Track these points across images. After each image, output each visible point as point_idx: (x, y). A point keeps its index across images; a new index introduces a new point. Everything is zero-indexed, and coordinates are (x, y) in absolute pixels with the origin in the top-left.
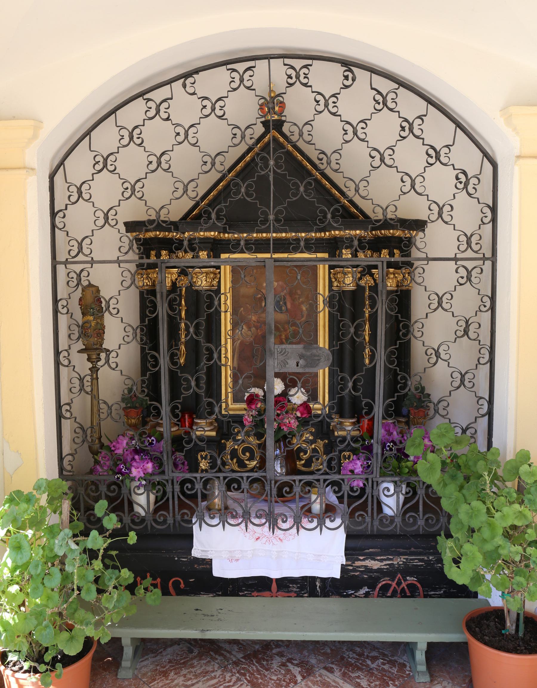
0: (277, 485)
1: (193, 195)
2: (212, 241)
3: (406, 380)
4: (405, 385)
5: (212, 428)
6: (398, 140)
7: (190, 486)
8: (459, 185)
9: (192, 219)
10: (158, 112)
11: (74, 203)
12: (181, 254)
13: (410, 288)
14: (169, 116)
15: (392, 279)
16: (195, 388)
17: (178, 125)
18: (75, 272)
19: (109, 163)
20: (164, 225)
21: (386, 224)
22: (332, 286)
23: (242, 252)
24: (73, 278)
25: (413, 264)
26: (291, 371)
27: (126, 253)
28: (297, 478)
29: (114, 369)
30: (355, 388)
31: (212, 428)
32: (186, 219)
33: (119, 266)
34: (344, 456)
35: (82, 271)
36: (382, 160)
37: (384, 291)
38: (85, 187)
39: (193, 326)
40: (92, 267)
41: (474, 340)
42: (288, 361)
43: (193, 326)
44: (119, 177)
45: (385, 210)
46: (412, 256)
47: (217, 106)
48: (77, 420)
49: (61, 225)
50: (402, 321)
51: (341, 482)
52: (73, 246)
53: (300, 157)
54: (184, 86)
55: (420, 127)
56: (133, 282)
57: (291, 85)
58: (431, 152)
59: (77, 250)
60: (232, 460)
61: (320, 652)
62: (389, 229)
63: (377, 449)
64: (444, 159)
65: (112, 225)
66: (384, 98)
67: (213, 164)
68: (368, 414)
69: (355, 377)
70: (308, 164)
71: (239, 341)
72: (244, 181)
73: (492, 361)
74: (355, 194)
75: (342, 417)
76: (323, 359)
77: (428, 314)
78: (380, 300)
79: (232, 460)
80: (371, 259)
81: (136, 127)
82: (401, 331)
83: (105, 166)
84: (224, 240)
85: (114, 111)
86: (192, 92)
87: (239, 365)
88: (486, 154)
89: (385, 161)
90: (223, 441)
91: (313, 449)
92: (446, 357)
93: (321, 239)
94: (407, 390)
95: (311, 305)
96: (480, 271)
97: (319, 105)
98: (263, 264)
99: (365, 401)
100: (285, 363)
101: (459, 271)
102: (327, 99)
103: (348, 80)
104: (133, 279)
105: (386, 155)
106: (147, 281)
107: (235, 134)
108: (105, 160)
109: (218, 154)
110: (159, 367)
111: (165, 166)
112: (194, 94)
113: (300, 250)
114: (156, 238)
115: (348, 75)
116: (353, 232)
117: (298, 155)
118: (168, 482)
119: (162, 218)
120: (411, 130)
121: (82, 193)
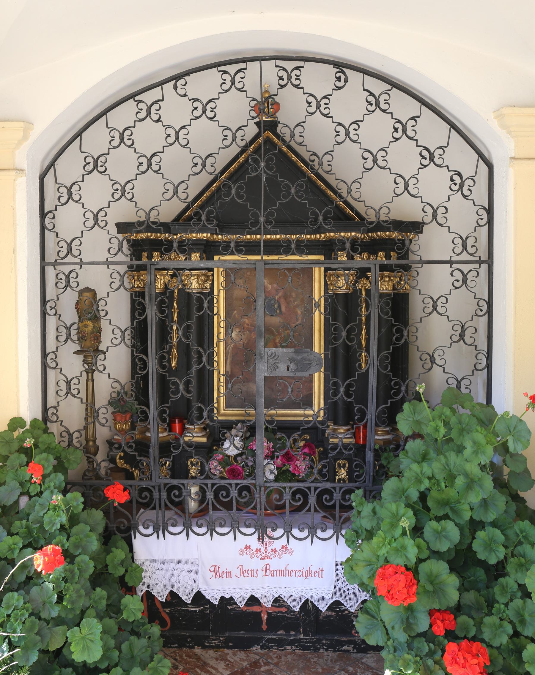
1: (184, 196)
2: (205, 242)
5: (204, 434)
6: (391, 142)
7: (177, 492)
8: (453, 187)
9: (184, 220)
10: (149, 113)
11: (63, 204)
12: (173, 255)
14: (160, 118)
16: (184, 393)
17: (168, 126)
18: (64, 273)
19: (99, 164)
20: (154, 226)
21: (379, 226)
22: (328, 289)
23: (232, 254)
24: (61, 279)
25: (411, 266)
26: (281, 375)
27: (115, 255)
28: (287, 485)
29: (101, 372)
30: (347, 393)
31: (204, 434)
32: (178, 221)
33: (108, 268)
34: (339, 464)
35: (71, 272)
36: (375, 161)
38: (75, 188)
40: (81, 268)
41: (471, 345)
42: (278, 365)
44: (110, 178)
45: (378, 212)
46: (409, 259)
47: (208, 107)
48: (63, 424)
49: (50, 226)
50: (396, 325)
51: (333, 490)
52: (62, 247)
53: (294, 158)
54: (175, 87)
55: (413, 128)
56: (122, 284)
57: (283, 86)
59: (66, 251)
61: (311, 671)
62: (385, 232)
64: (438, 161)
65: (102, 226)
67: (204, 166)
68: (361, 420)
69: (347, 382)
70: (303, 165)
71: (233, 345)
72: (235, 183)
73: (489, 367)
75: (335, 424)
76: (314, 364)
77: (423, 319)
78: (373, 304)
80: (368, 262)
81: (127, 129)
82: (394, 335)
83: (96, 167)
84: (218, 242)
85: (105, 113)
86: (183, 93)
87: (231, 369)
88: (481, 155)
90: (214, 448)
92: (441, 363)
93: (316, 241)
96: (476, 274)
97: (311, 106)
98: (253, 266)
99: (357, 407)
102: (319, 100)
103: (340, 81)
104: (122, 281)
105: (379, 157)
106: (138, 283)
107: (226, 136)
108: (96, 161)
109: (209, 156)
111: (155, 167)
112: (185, 95)
113: (291, 253)
115: (340, 77)
116: (348, 234)
117: (293, 156)
118: (155, 488)
119: (152, 219)
120: (404, 131)
121: (72, 194)
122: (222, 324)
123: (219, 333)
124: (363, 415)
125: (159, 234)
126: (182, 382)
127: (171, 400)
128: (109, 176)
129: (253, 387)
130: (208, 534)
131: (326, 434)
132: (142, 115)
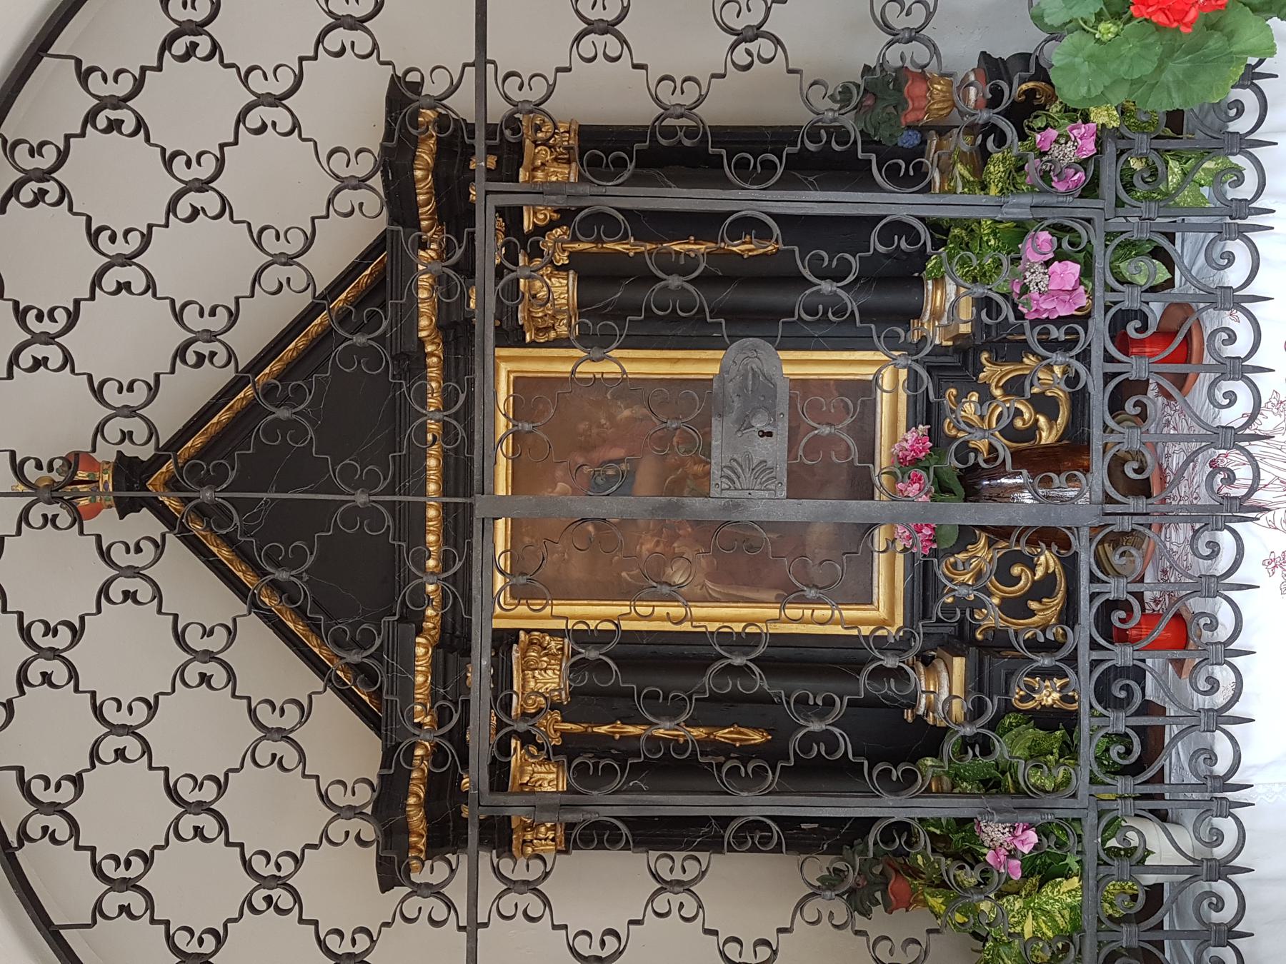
0: (1119, 497)
5: (941, 666)
14: (68, 778)
15: (547, 175)
17: (94, 756)
27: (450, 905)
29: (775, 952)
31: (941, 666)
33: (485, 925)
36: (203, 186)
37: (587, 189)
42: (755, 462)
47: (45, 642)
53: (223, 416)
58: (180, 47)
60: (1032, 613)
62: (413, 181)
63: (1018, 206)
66: (28, 177)
69: (806, 273)
71: (709, 584)
74: (299, 265)
75: (918, 314)
79: (1032, 613)
90: (979, 637)
91: (1006, 393)
93: (445, 365)
95: (616, 397)
100: (764, 468)
102: (29, 337)
104: (523, 888)
106: (543, 829)
110: (769, 822)
111: (210, 791)
114: (428, 805)
117: (215, 420)
122: (646, 611)
123: (668, 618)
124: (899, 227)
125: (414, 775)
127: (850, 756)
129: (818, 535)
130: (1238, 661)
131: (944, 343)
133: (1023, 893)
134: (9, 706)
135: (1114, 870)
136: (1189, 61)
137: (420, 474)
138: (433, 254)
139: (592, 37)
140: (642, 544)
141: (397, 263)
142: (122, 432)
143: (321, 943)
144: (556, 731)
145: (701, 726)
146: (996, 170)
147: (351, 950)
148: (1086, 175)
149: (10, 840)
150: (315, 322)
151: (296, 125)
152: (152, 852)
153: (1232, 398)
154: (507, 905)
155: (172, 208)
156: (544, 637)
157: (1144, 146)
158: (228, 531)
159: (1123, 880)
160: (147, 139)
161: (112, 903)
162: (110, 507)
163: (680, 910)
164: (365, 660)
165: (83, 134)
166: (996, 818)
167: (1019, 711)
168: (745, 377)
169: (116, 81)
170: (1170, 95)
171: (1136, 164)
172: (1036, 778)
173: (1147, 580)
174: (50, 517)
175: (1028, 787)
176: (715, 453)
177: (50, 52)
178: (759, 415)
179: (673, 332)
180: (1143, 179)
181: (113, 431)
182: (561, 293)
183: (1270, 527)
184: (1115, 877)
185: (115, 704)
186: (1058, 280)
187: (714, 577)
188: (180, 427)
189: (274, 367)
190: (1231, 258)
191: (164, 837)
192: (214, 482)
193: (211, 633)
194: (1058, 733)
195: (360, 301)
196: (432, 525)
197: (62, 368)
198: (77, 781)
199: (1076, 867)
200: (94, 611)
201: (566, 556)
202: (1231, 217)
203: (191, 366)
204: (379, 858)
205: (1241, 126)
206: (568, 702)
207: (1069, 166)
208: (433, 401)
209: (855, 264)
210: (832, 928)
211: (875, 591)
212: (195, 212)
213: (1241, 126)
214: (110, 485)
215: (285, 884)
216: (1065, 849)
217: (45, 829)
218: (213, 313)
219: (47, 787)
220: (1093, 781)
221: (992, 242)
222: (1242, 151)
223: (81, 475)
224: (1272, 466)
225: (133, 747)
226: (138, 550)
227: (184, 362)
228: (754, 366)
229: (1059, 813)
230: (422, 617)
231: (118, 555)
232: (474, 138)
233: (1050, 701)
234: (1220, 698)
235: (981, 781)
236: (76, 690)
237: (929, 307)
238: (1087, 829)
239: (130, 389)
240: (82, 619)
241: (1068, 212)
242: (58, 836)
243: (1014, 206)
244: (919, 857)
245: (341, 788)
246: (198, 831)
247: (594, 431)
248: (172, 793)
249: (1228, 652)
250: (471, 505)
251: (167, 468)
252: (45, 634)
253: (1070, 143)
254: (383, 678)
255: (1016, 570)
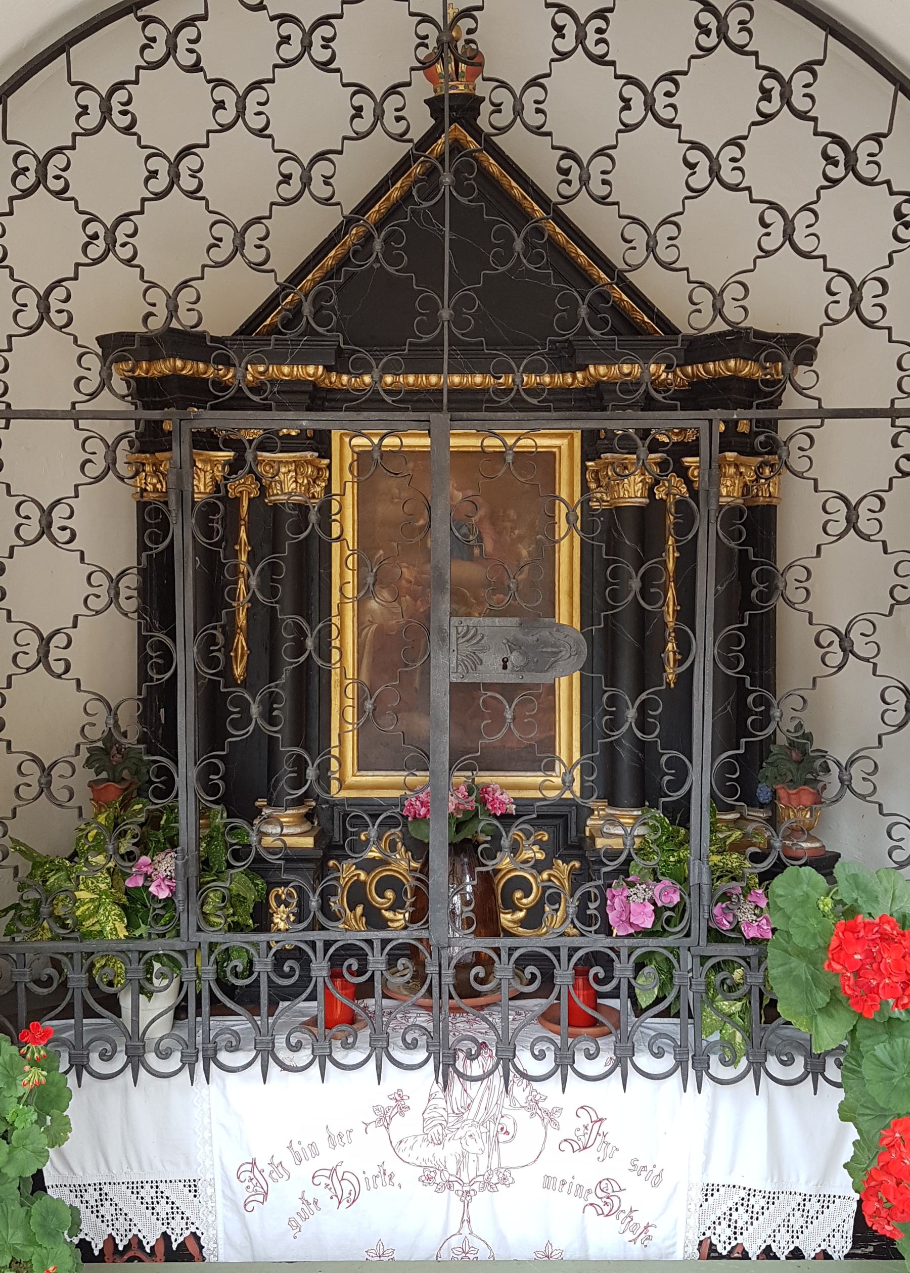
3: (769, 705)
4: (765, 720)
10: (172, 50)
13: (775, 501)
17: (220, 82)
19: (52, 171)
27: (93, 395)
29: (59, 676)
30: (643, 724)
31: (306, 827)
33: (77, 426)
36: (715, 172)
37: (713, 507)
39: (257, 572)
42: (481, 655)
43: (257, 572)
47: (317, 38)
53: (517, 191)
55: (807, 90)
60: (352, 909)
62: (725, 359)
63: (700, 873)
66: (722, 21)
69: (643, 696)
71: (374, 627)
74: (647, 257)
75: (612, 804)
76: (565, 654)
79: (352, 909)
83: (41, 179)
85: (62, 47)
89: (722, 173)
90: (331, 863)
93: (566, 390)
94: (769, 731)
95: (539, 543)
101: (900, 442)
102: (582, 22)
105: (724, 160)
106: (155, 481)
108: (43, 164)
110: (172, 670)
114: (175, 377)
117: (514, 184)
120: (786, 99)
126: (258, 698)
128: (76, 203)
129: (419, 723)
130: (315, 1069)
131: (587, 829)
132: (156, 52)
133: (113, 890)
134: (260, 7)
135: (135, 965)
136: (807, 978)
137: (468, 368)
138: (664, 376)
139: (844, 510)
140: (408, 568)
141: (653, 345)
142: (501, 104)
143: (58, 283)
144: (241, 492)
145: (247, 621)
146: (733, 860)
147: (53, 310)
148: (727, 930)
149: (143, 9)
150: (601, 273)
151: (768, 254)
152: (135, 134)
153: (540, 1057)
154: (94, 445)
155: (695, 146)
156: (324, 481)
157: (753, 980)
158: (416, 197)
159: (126, 972)
160: (754, 124)
161: (90, 99)
162: (435, 91)
163: (94, 595)
164: (305, 319)
165: (758, 67)
166: (180, 862)
167: (268, 894)
168: (554, 645)
169: (804, 96)
170: (781, 965)
171: (738, 974)
172: (214, 898)
173: (386, 1002)
174: (426, 41)
175: (205, 891)
176: (488, 621)
177: (829, 36)
178: (521, 658)
179: (595, 592)
180: (724, 979)
181: (502, 95)
182: (628, 492)
183: (430, 1095)
184: (128, 967)
185: (263, 100)
186: (639, 910)
187: (380, 632)
188: (507, 153)
189: (561, 236)
190: (659, 1055)
191: (148, 144)
192: (458, 185)
193: (327, 183)
194: (251, 922)
195: (617, 310)
196: (423, 379)
197: (556, 51)
198: (196, 68)
199: (137, 933)
200: (344, 81)
201: (396, 500)
202: (694, 1055)
203: (558, 164)
204: (132, 335)
205: (773, 1064)
206: (266, 504)
207: (735, 916)
208: (531, 380)
209: (649, 738)
210: (81, 725)
211: (370, 773)
212: (692, 166)
213: (773, 1064)
214: (455, 91)
215: (109, 250)
216: (153, 924)
217: (154, 40)
218: (605, 182)
219: (191, 41)
220: (212, 946)
221: (672, 859)
222: (751, 1064)
223: (463, 67)
224: (483, 1096)
225: (225, 116)
226: (398, 119)
227: (562, 157)
228: (563, 653)
229: (184, 917)
230: (340, 373)
231: (394, 101)
232: (757, 408)
233: (276, 920)
234: (284, 1054)
235: (207, 859)
236: (276, 66)
237: (618, 812)
238: (171, 941)
239: (538, 111)
240: (338, 70)
241: (695, 915)
242: (147, 51)
243: (700, 869)
244: (141, 806)
245: (194, 299)
246: (153, 174)
247: (508, 524)
248: (187, 151)
249: (323, 1059)
250: (439, 410)
251: (471, 142)
252: (323, 38)
253: (754, 917)
254: (290, 334)
255: (390, 894)
